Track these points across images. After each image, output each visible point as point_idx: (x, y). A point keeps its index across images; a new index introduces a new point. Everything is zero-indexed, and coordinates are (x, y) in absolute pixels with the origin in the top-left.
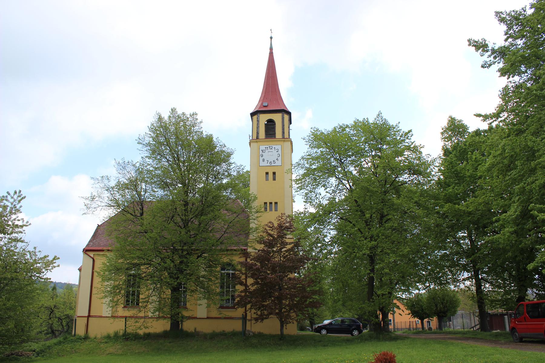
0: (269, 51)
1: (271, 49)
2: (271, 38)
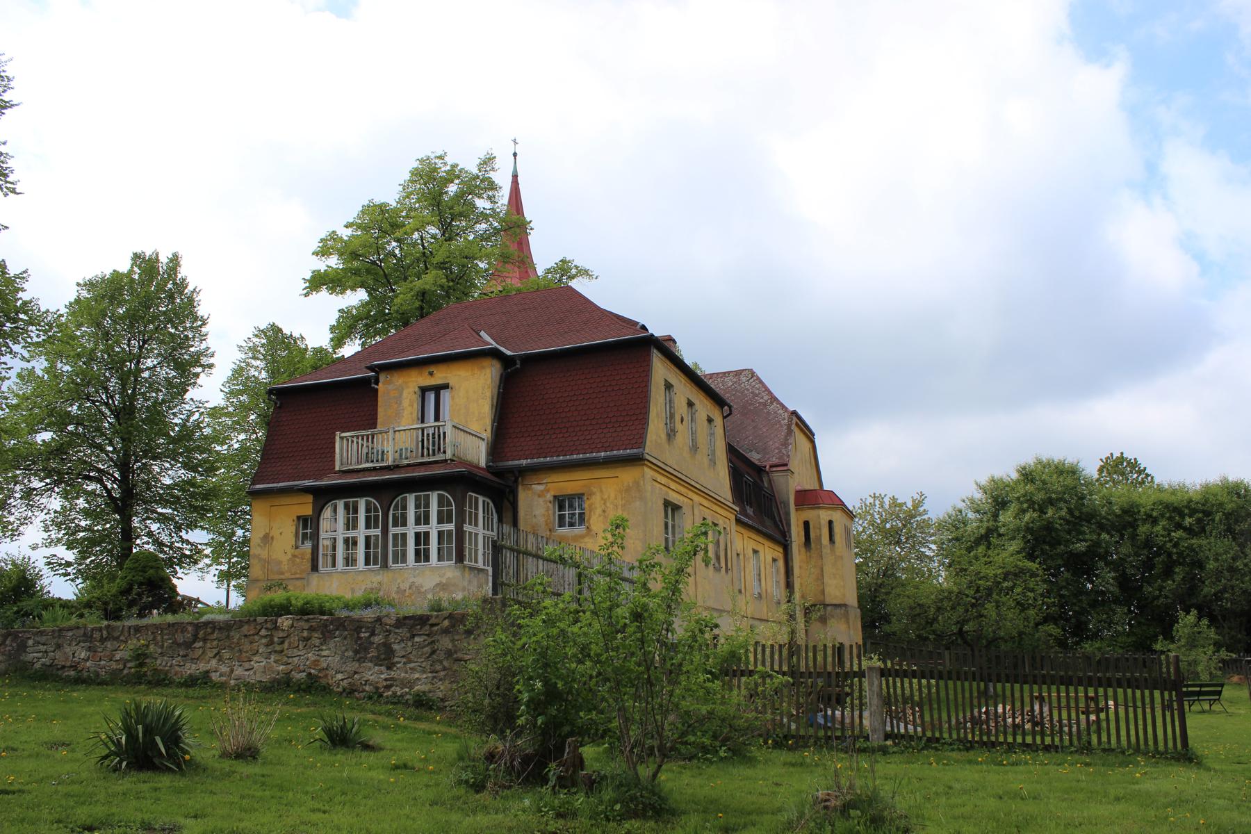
0: (510, 179)
1: (515, 177)
2: (515, 155)
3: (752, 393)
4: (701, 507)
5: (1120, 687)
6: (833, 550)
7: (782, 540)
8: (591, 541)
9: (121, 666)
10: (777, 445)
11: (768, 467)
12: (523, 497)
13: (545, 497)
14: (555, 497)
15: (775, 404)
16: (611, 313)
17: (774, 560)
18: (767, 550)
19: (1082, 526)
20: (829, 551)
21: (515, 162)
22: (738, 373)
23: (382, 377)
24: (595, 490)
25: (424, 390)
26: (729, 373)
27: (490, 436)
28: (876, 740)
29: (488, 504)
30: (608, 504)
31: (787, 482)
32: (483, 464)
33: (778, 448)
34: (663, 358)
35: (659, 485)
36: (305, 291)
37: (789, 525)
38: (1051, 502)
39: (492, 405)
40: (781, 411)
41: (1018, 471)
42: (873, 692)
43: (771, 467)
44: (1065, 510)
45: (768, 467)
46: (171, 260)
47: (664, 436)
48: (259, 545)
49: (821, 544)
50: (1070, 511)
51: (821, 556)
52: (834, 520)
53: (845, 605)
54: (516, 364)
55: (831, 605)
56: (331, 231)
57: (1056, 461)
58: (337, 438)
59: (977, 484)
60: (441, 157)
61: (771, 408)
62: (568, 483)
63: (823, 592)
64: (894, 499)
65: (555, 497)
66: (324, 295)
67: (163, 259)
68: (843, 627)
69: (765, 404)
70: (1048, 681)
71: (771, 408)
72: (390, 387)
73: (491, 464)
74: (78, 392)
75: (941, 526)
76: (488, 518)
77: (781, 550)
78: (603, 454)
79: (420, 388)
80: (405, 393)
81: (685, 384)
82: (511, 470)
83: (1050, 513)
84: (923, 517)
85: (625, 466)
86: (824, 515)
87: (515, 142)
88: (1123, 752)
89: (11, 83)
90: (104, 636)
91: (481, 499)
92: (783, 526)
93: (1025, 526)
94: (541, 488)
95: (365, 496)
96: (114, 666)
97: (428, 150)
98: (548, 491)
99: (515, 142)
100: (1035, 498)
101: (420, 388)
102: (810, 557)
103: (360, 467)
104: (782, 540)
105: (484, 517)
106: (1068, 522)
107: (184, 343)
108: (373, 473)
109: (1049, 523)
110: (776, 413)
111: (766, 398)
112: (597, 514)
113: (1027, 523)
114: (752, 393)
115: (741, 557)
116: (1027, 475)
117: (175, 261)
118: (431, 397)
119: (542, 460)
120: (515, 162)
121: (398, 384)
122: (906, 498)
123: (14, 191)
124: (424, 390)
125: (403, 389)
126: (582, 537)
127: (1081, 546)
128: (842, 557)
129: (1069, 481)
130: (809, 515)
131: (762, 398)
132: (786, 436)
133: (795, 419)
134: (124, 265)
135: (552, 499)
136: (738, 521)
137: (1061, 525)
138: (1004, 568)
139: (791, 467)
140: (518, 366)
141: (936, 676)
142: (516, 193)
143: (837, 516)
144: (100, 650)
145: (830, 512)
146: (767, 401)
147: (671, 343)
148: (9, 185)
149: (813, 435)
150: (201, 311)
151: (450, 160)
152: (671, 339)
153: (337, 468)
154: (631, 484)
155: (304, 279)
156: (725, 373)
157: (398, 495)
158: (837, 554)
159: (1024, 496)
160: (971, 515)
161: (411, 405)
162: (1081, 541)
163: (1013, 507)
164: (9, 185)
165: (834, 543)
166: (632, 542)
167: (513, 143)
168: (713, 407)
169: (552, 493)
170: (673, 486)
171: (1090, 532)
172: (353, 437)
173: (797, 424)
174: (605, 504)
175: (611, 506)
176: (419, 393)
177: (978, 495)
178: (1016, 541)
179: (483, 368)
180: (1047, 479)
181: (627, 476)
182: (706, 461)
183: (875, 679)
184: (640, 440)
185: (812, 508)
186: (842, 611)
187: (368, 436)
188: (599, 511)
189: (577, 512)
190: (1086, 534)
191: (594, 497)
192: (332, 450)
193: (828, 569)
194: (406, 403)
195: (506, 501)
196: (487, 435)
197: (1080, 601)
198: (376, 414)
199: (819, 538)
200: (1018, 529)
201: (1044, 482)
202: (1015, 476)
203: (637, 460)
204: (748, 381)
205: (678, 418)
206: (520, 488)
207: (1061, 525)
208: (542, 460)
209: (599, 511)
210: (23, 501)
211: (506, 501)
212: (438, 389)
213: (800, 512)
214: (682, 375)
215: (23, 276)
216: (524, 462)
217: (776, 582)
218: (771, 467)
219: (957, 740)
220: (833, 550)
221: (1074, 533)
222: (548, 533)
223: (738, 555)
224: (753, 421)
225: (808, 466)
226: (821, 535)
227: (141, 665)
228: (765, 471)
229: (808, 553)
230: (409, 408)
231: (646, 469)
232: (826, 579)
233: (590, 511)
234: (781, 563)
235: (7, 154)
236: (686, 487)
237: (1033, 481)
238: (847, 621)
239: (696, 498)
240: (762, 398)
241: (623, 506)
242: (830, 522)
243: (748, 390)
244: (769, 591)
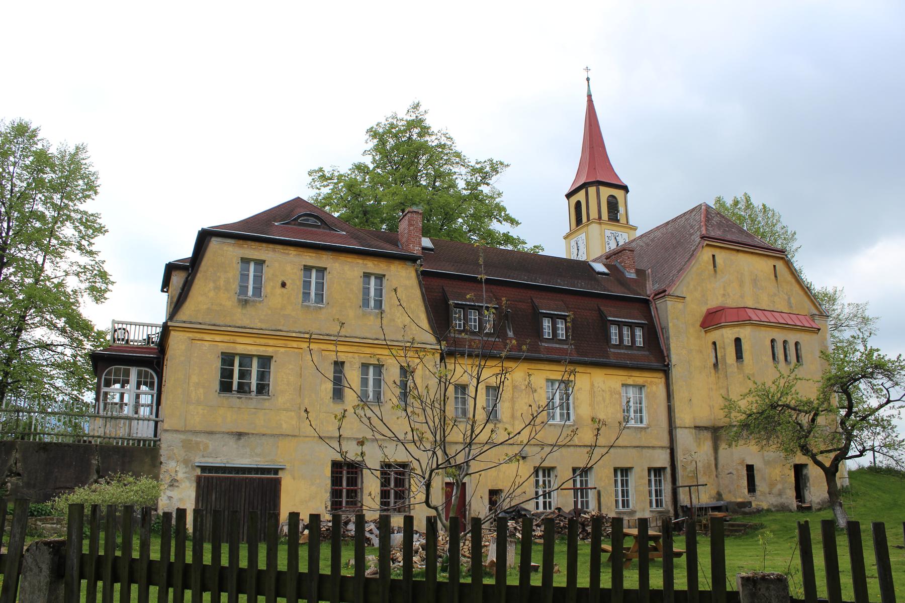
1: (589, 96)
2: (588, 79)
16: (285, 203)
20: (736, 370)
26: (669, 221)
49: (726, 363)
51: (726, 376)
52: (741, 337)
87: (587, 69)
97: (26, 119)
99: (587, 69)
102: (718, 377)
130: (715, 335)
145: (736, 330)
158: (747, 372)
170: (218, 338)
199: (724, 357)
210: (772, 439)
215: (718, 200)
220: (740, 369)
229: (717, 375)
236: (228, 335)
242: (738, 341)
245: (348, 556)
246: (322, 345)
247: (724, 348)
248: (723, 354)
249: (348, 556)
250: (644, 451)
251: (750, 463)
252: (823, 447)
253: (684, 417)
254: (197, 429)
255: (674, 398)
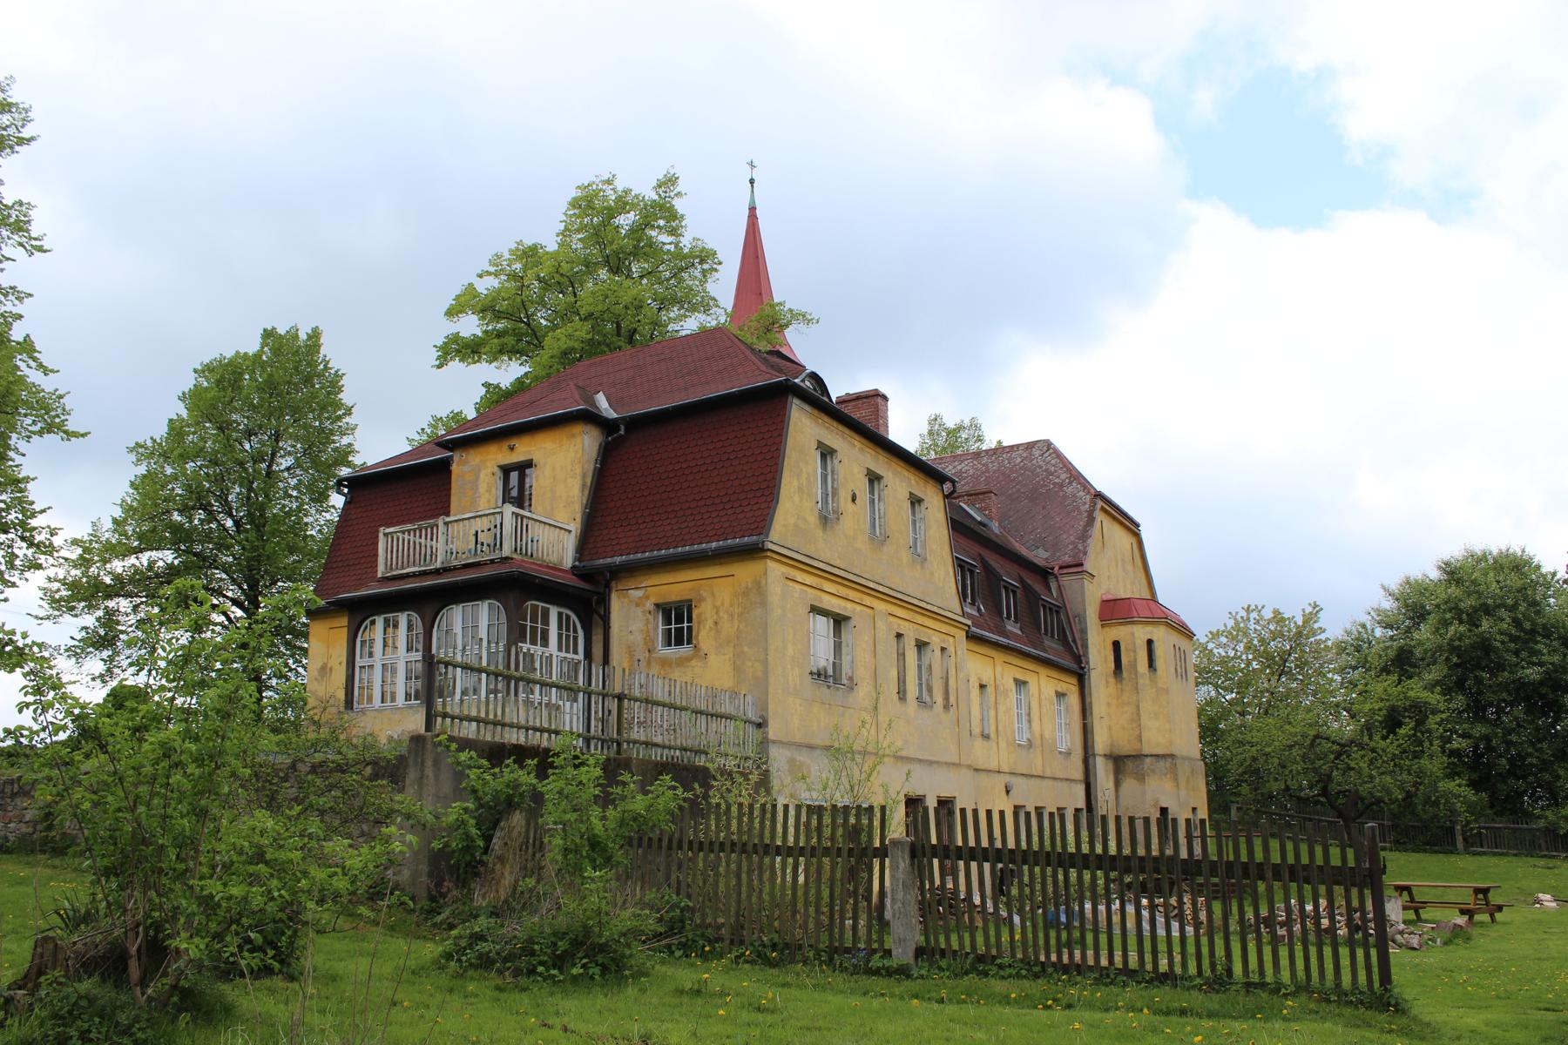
1: (752, 210)
2: (752, 182)
3: (1046, 470)
4: (891, 618)
5: (1294, 881)
6: (1153, 681)
7: (1074, 666)
8: (699, 664)
9: (30, 830)
10: (1072, 538)
11: (1056, 569)
12: (617, 605)
13: (644, 606)
14: (657, 606)
15: (1074, 484)
17: (1060, 695)
18: (1044, 680)
19: (1537, 643)
20: (1148, 682)
21: (753, 191)
22: (1030, 446)
23: (456, 457)
24: (705, 594)
25: (506, 470)
27: (579, 526)
28: (902, 955)
29: (568, 617)
30: (721, 614)
31: (1082, 586)
32: (568, 561)
33: (1073, 543)
34: (816, 412)
35: (798, 587)
36: (438, 362)
37: (1085, 646)
38: (1487, 610)
39: (584, 485)
40: (1082, 493)
41: (1439, 568)
42: (898, 880)
43: (1061, 568)
44: (1508, 620)
45: (1056, 569)
46: (310, 337)
47: (813, 519)
48: (316, 679)
50: (1517, 622)
51: (1137, 688)
52: (1154, 638)
53: (1172, 756)
54: (619, 430)
55: (1152, 756)
56: (466, 284)
57: (1495, 552)
58: (381, 535)
59: (1384, 589)
60: (609, 182)
61: (1069, 490)
62: (673, 586)
63: (1140, 737)
64: (1277, 613)
65: (657, 606)
66: (455, 365)
67: (303, 336)
68: (1168, 785)
69: (1061, 486)
70: (1093, 865)
71: (1069, 490)
72: (466, 468)
73: (577, 563)
74: (197, 499)
75: (1341, 648)
76: (568, 637)
77: (1074, 681)
78: (714, 545)
79: (501, 467)
80: (482, 476)
81: (861, 449)
82: (600, 571)
83: (1485, 625)
84: (1318, 638)
85: (742, 561)
86: (1141, 633)
87: (752, 165)
88: (1277, 990)
89: (30, 114)
90: (15, 791)
91: (554, 612)
92: (1077, 648)
93: (1449, 644)
94: (639, 593)
95: (407, 610)
96: (24, 829)
97: (589, 173)
98: (647, 597)
99: (752, 165)
100: (1462, 605)
101: (501, 467)
102: (1122, 690)
103: (405, 571)
104: (1074, 666)
105: (560, 636)
106: (1513, 639)
107: (325, 436)
108: (429, 577)
109: (1484, 640)
110: (1074, 495)
111: (1064, 476)
112: (707, 627)
113: (1451, 640)
114: (1046, 470)
115: (990, 690)
116: (1452, 573)
117: (315, 335)
118: (514, 476)
119: (639, 555)
120: (753, 191)
121: (473, 463)
122: (1294, 612)
123: (41, 249)
124: (506, 470)
125: (480, 470)
126: (689, 659)
127: (1533, 673)
128: (1166, 691)
129: (1514, 581)
130: (1119, 632)
131: (1058, 477)
132: (1085, 527)
133: (1100, 503)
134: (251, 345)
135: (652, 608)
136: (972, 637)
137: (1503, 643)
138: (1388, 700)
139: (1088, 566)
140: (622, 432)
141: (990, 859)
142: (754, 230)
143: (1160, 634)
144: (10, 808)
145: (1149, 628)
146: (1064, 481)
147: (879, 400)
148: (34, 243)
149: (1137, 525)
150: (346, 397)
151: (620, 185)
152: (876, 390)
153: (380, 575)
154: (750, 585)
155: (435, 346)
156: (1012, 447)
157: (443, 607)
158: (1160, 685)
159: (1446, 603)
160: (1379, 632)
161: (489, 491)
162: (1535, 664)
163: (1432, 619)
164: (34, 243)
165: (1155, 670)
166: (750, 664)
167: (749, 167)
168: (922, 483)
169: (653, 600)
170: (828, 587)
171: (1549, 652)
172: (403, 532)
173: (1103, 509)
174: (717, 613)
175: (726, 616)
176: (499, 474)
177: (1388, 604)
178: (1438, 666)
179: (573, 436)
180: (1482, 579)
181: (744, 572)
182: (905, 556)
183: (900, 860)
184: (763, 522)
185: (1121, 624)
186: (1168, 764)
187: (415, 530)
188: (710, 623)
189: (685, 625)
190: (1544, 655)
191: (703, 604)
192: (374, 552)
193: (1147, 707)
194: (482, 488)
195: (596, 617)
196: (575, 527)
197: (1540, 750)
198: (449, 506)
199: (1134, 664)
200: (1440, 648)
201: (1474, 582)
202: (1435, 574)
203: (755, 551)
204: (1042, 455)
205: (844, 496)
206: (614, 596)
207: (1503, 643)
208: (639, 555)
209: (710, 623)
211: (596, 617)
212: (524, 467)
213: (1107, 629)
214: (856, 436)
216: (618, 559)
217: (1066, 724)
218: (1061, 568)
219: (1022, 961)
220: (1153, 681)
221: (1524, 654)
222: (647, 654)
223: (982, 687)
224: (1044, 508)
225: (1129, 567)
226: (1135, 660)
227: (50, 827)
228: (1052, 574)
229: (1119, 686)
230: (487, 495)
231: (770, 563)
232: (1144, 720)
233: (699, 623)
234: (1074, 699)
235: (29, 204)
237: (1459, 582)
238: (1176, 779)
239: (881, 606)
240: (1058, 477)
241: (741, 615)
242: (1150, 642)
243: (1041, 467)
244: (1047, 735)
245: (1077, 954)
246: (938, 623)
247: (1135, 652)
248: (1132, 659)
249: (1077, 954)
250: (983, 776)
251: (1165, 806)
252: (324, 688)
253: (1101, 743)
254: (797, 740)
255: (1091, 714)
